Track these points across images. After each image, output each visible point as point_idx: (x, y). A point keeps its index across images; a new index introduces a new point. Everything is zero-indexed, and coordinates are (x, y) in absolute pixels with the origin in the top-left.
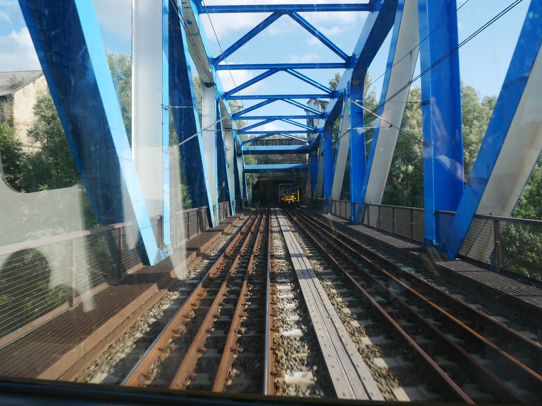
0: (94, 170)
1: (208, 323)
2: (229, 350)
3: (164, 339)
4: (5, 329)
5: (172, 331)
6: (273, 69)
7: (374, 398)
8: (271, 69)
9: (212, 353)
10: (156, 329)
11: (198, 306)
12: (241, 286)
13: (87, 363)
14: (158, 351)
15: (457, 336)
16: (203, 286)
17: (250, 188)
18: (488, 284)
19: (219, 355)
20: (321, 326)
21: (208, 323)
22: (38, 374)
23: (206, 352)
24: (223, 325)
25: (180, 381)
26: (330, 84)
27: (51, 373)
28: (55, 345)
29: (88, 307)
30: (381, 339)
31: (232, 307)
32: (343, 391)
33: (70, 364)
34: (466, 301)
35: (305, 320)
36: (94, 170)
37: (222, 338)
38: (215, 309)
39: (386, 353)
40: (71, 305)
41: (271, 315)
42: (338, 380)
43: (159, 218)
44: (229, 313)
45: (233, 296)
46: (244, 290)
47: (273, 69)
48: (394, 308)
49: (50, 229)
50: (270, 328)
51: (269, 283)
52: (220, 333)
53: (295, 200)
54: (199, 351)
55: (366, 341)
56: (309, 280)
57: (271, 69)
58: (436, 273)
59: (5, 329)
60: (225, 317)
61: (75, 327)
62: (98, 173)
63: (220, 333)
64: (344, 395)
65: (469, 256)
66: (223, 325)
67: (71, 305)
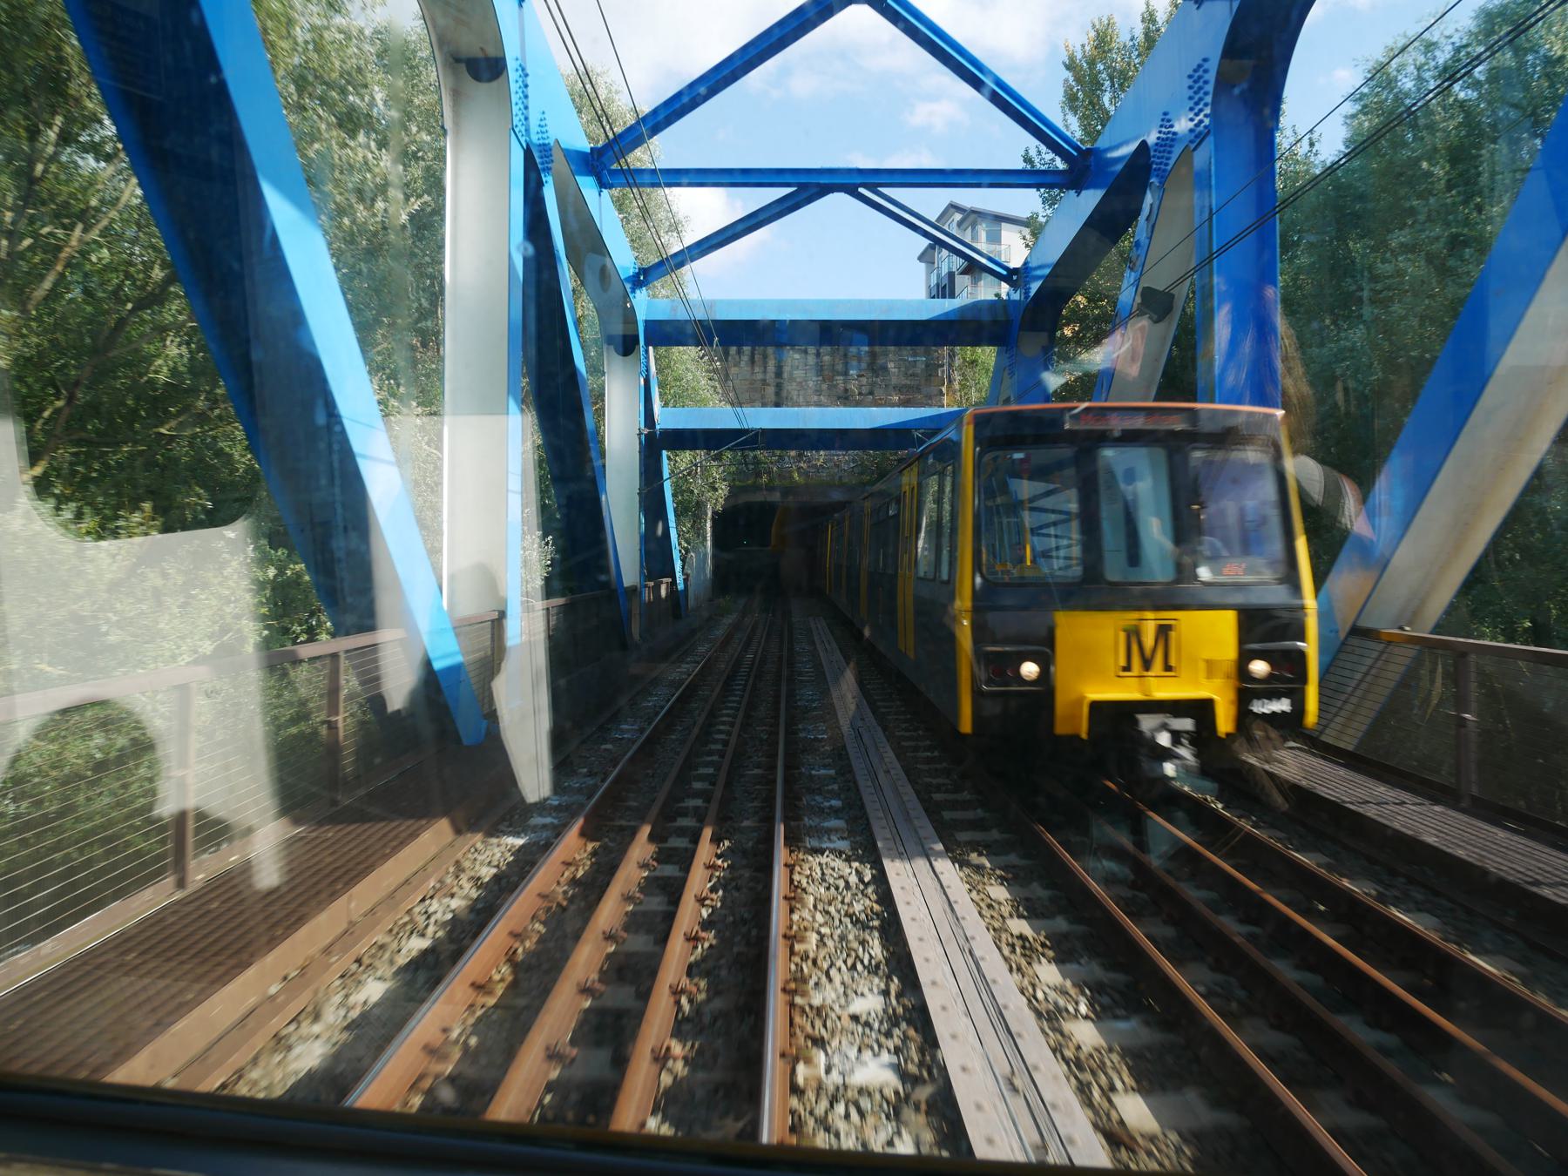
0: (323, 482)
1: (586, 960)
2: (682, 938)
3: (487, 958)
4: (13, 934)
5: (473, 985)
6: (807, 187)
7: (1081, 1160)
8: (802, 187)
9: (639, 943)
10: (463, 933)
11: (500, 990)
12: (695, 840)
13: (259, 1033)
14: (470, 991)
15: (1303, 965)
16: (583, 834)
17: (698, 530)
18: (1460, 853)
19: (671, 908)
20: (944, 986)
21: (586, 960)
22: (123, 1054)
23: (601, 994)
24: (632, 973)
25: (516, 1099)
26: (1068, 67)
27: (145, 1068)
28: (161, 984)
29: (268, 876)
30: (1130, 1027)
31: (650, 948)
32: (993, 1132)
33: (198, 1044)
34: (1381, 898)
35: (913, 1016)
36: (323, 482)
37: (686, 849)
38: (610, 912)
39: (1151, 1076)
40: (181, 884)
41: (785, 898)
42: (979, 1107)
43: (495, 615)
44: (658, 926)
45: (670, 870)
46: (705, 851)
47: (807, 187)
48: (419, 196)
49: (162, 641)
50: (782, 930)
51: (781, 854)
52: (622, 996)
53: (1247, 690)
54: (553, 1055)
55: (1048, 973)
56: (921, 864)
57: (802, 187)
58: (1279, 799)
59: (13, 934)
60: (657, 900)
61: (223, 933)
62: (337, 490)
63: (622, 996)
64: (990, 1141)
65: (1323, 738)
66: (632, 973)
67: (181, 884)
